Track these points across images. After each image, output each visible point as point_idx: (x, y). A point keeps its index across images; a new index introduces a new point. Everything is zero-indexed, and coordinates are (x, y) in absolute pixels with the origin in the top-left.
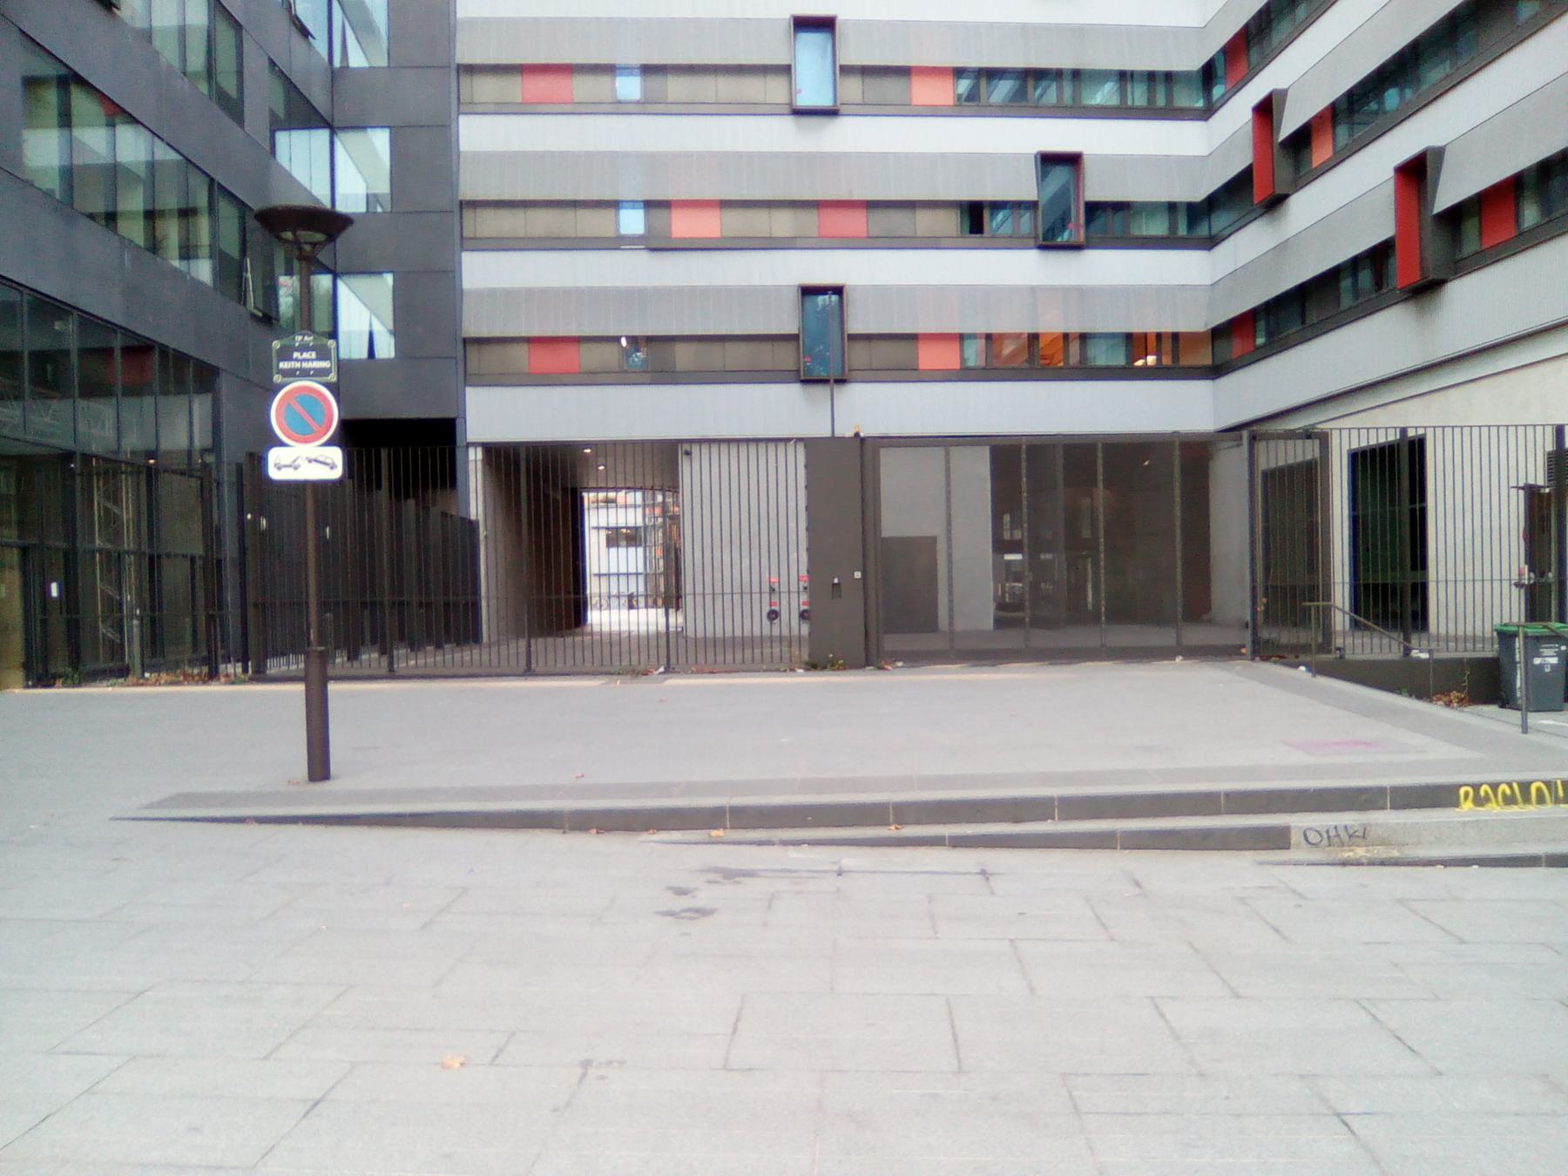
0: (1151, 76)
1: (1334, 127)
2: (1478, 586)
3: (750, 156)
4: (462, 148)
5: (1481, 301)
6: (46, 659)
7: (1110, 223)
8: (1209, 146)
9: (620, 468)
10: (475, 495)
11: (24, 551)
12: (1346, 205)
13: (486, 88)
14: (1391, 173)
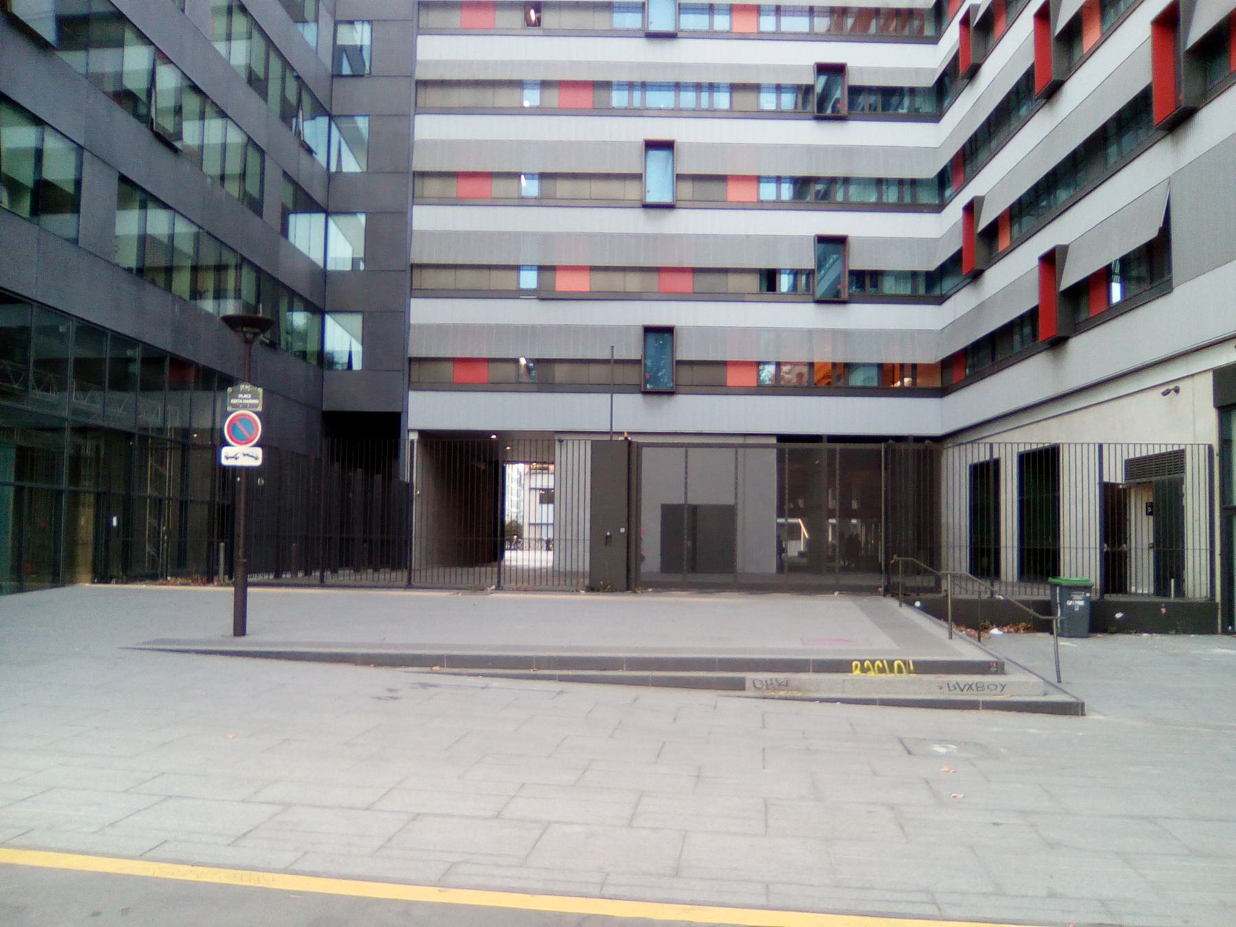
0: (901, 182)
1: (1011, 226)
2: (1086, 551)
3: (612, 235)
4: (415, 228)
5: (1091, 353)
6: (106, 567)
7: (866, 284)
8: (934, 232)
9: (527, 449)
10: (413, 467)
11: (98, 496)
12: (1011, 281)
13: (433, 187)
14: (1036, 262)
